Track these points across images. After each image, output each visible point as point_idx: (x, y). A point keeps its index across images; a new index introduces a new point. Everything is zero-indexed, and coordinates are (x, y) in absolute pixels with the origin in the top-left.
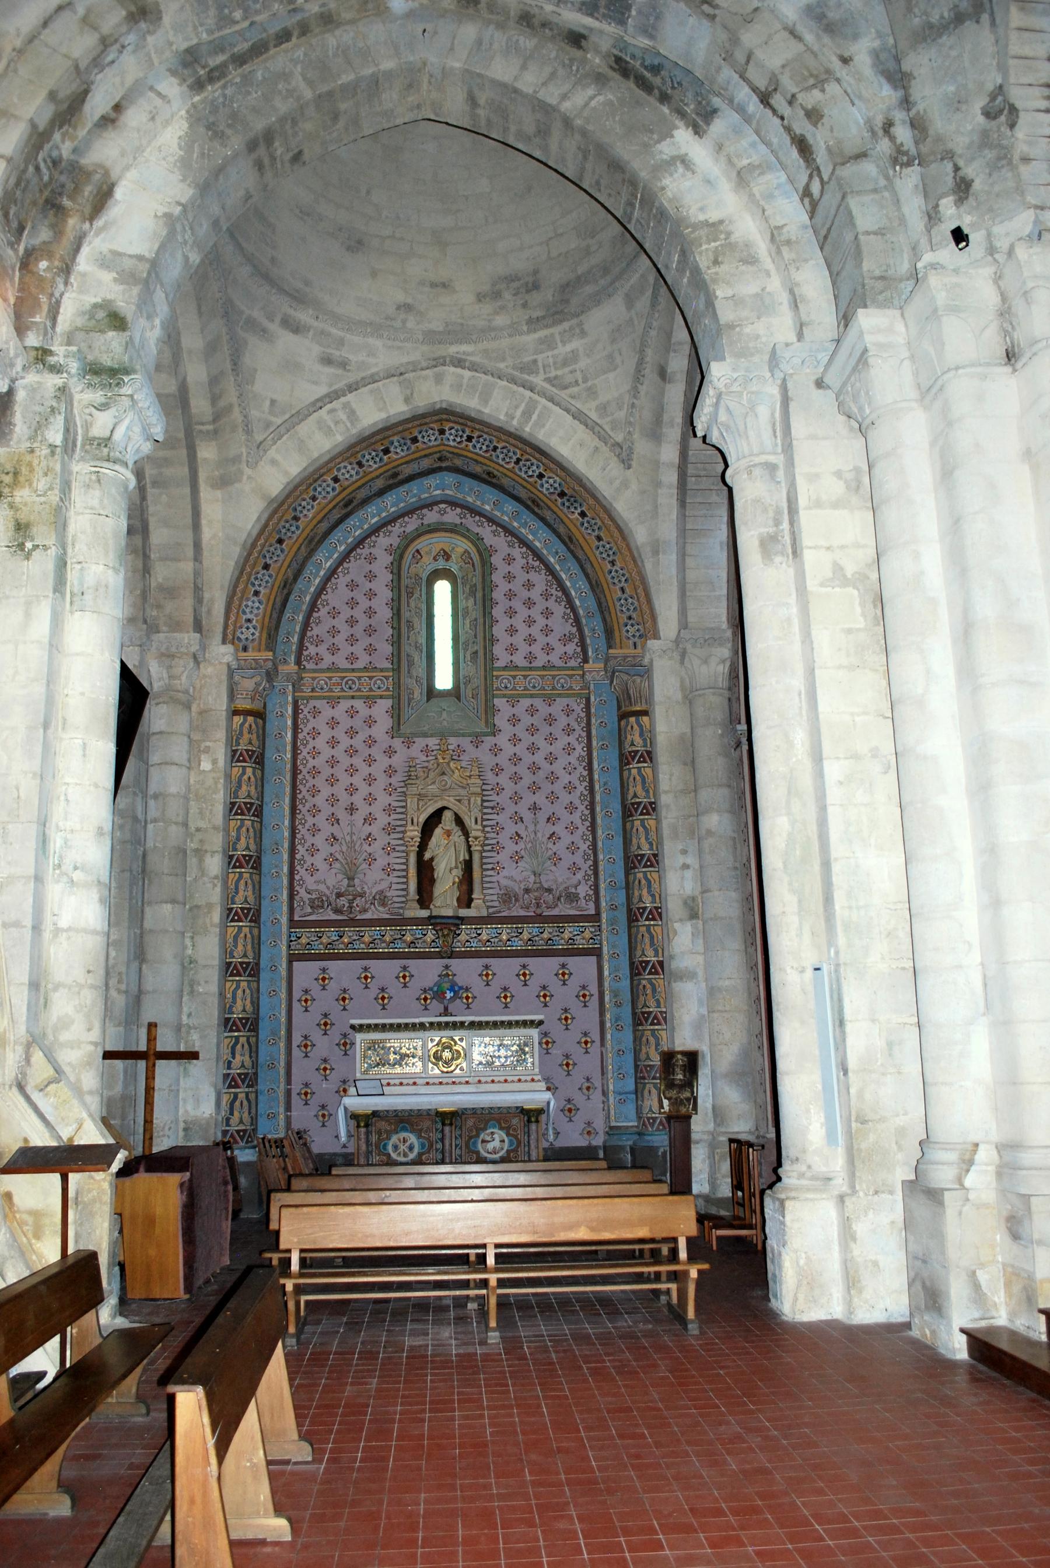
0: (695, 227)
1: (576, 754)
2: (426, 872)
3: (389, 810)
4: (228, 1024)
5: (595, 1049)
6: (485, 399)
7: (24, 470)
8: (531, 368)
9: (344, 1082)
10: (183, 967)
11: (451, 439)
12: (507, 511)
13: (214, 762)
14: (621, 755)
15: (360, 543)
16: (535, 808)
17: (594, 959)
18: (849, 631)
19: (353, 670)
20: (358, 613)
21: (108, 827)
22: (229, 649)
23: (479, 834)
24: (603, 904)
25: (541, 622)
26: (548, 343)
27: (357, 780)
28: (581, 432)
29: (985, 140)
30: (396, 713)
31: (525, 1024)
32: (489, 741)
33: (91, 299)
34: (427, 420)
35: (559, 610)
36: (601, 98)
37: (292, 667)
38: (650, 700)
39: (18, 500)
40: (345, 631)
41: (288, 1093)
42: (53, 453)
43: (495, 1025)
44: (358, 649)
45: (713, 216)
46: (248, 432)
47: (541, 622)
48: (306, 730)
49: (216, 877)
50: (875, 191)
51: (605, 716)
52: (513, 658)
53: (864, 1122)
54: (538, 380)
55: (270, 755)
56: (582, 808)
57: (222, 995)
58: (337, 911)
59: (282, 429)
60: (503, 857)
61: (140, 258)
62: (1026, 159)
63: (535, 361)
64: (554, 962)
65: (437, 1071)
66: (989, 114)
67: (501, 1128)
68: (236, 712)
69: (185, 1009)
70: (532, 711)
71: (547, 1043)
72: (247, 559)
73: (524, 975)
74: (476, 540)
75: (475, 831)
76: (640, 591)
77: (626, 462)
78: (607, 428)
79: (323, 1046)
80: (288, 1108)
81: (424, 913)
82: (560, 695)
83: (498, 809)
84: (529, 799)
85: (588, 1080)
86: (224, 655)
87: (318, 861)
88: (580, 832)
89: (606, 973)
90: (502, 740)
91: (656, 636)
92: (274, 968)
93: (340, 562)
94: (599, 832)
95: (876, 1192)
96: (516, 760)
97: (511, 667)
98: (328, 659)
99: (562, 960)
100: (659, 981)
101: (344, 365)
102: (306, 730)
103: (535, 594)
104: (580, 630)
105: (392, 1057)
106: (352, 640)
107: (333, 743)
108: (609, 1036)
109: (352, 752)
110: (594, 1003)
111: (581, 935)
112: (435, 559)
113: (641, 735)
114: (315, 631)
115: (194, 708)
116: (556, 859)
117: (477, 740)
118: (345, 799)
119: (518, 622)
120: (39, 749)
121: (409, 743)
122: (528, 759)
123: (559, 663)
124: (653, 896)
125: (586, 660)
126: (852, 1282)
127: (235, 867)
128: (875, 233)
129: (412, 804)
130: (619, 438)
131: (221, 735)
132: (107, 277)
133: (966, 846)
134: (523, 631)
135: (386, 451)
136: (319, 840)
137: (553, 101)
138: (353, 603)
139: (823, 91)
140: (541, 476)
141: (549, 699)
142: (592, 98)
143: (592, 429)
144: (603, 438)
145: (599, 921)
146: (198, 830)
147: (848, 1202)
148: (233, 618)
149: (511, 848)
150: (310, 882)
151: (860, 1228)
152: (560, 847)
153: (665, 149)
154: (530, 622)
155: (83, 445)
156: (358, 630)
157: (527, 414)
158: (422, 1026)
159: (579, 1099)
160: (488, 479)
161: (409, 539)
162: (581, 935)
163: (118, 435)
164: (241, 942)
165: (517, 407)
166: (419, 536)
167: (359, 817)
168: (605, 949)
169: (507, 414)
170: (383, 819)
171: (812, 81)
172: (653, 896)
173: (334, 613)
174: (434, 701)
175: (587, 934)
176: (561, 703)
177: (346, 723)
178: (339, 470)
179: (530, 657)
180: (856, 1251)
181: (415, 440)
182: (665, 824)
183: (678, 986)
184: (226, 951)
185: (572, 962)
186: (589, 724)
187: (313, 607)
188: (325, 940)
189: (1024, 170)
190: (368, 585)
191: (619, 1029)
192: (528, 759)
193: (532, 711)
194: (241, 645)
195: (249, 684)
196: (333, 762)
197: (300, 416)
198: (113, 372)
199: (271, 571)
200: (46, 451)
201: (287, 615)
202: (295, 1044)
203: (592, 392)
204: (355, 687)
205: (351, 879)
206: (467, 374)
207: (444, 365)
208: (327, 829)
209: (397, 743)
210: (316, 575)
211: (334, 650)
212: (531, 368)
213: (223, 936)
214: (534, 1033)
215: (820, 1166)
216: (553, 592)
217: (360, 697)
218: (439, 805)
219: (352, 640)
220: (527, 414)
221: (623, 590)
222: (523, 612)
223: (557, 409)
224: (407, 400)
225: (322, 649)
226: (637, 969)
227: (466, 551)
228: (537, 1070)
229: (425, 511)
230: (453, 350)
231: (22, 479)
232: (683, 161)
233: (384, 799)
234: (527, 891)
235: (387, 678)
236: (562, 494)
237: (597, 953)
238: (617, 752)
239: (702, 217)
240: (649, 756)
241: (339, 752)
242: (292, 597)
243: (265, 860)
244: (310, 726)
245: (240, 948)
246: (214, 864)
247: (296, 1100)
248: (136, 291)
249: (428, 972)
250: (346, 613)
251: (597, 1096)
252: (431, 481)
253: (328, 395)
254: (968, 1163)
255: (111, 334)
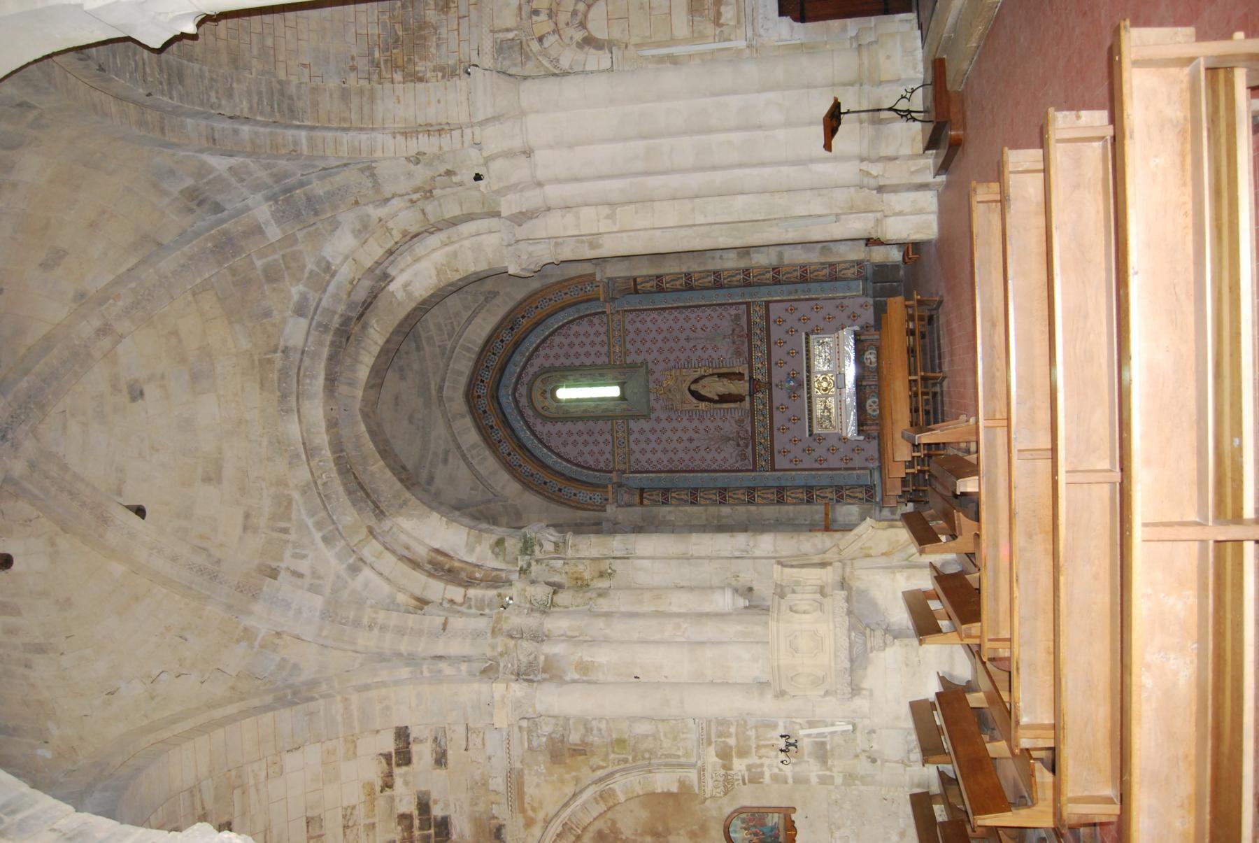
0: (439, 281)
1: (656, 317)
2: (724, 398)
3: (691, 420)
4: (810, 501)
5: (820, 303)
6: (460, 373)
7: (575, 575)
8: (443, 348)
9: (840, 439)
10: (780, 524)
11: (483, 391)
12: (519, 359)
13: (670, 512)
14: (659, 292)
15: (540, 441)
16: (688, 339)
17: (770, 305)
18: (636, 212)
19: (613, 441)
20: (580, 440)
21: (730, 534)
22: (608, 508)
23: (703, 370)
24: (741, 300)
25: (582, 338)
26: (430, 339)
27: (675, 438)
28: (478, 320)
29: (430, 164)
30: (637, 417)
31: (807, 343)
32: (650, 365)
33: (490, 554)
34: (472, 405)
35: (574, 328)
36: (375, 326)
37: (614, 475)
38: (629, 278)
39: (589, 577)
40: (591, 447)
41: (846, 469)
42: (567, 564)
43: (808, 359)
44: (601, 439)
45: (434, 272)
46: (489, 501)
47: (582, 338)
48: (647, 466)
49: (732, 509)
50: (440, 205)
51: (634, 302)
52: (603, 353)
53: (852, 207)
54: (449, 344)
55: (663, 484)
56: (687, 313)
57: (794, 504)
58: (747, 446)
59: (485, 484)
60: (715, 356)
61: (468, 534)
62: (440, 148)
63: (440, 346)
64: (773, 327)
65: (833, 390)
66: (418, 162)
67: (864, 354)
68: (641, 503)
69: (803, 522)
70: (633, 342)
71: (818, 330)
72: (558, 501)
73: (780, 343)
74: (536, 376)
75: (701, 372)
76: (566, 284)
77: (496, 294)
78: (476, 305)
79: (820, 451)
80: (854, 469)
81: (747, 399)
82: (624, 327)
83: (688, 361)
84: (683, 343)
85: (837, 307)
86: (612, 509)
87: (719, 457)
88: (701, 314)
89: (779, 298)
90: (650, 358)
91: (593, 275)
92: (779, 478)
93: (552, 451)
94: (701, 303)
95: (882, 201)
96: (661, 351)
97: (608, 355)
98: (608, 456)
99: (772, 322)
100: (783, 270)
101: (447, 452)
102: (647, 466)
103: (566, 342)
104: (586, 316)
105: (826, 414)
106: (596, 443)
107: (654, 451)
108: (814, 296)
109: (659, 441)
110: (795, 304)
111: (758, 312)
112: (546, 398)
113: (648, 282)
114: (592, 463)
115: (641, 524)
116: (716, 327)
117: (650, 372)
118: (686, 444)
119: (582, 351)
120: (700, 561)
121: (653, 410)
122: (660, 344)
123: (605, 327)
124: (737, 274)
125: (604, 313)
126: (920, 212)
127: (725, 500)
128: (461, 206)
129: (686, 407)
130: (483, 298)
131: (656, 510)
132: (478, 549)
133: (738, 172)
134: (587, 348)
135: (492, 427)
136: (709, 457)
137: (378, 349)
138: (575, 443)
139: (392, 229)
140: (502, 341)
141: (626, 332)
142: (376, 330)
143: (477, 313)
144: (481, 307)
145: (750, 302)
146: (707, 520)
147: (886, 213)
148: (589, 507)
149: (710, 352)
150: (731, 461)
151: (897, 209)
152: (709, 324)
153: (400, 295)
154: (582, 344)
155: (558, 554)
156: (590, 439)
157: (468, 350)
158: (810, 398)
159: (848, 312)
160: (502, 370)
161: (537, 414)
162: (758, 312)
163: (553, 539)
164: (766, 496)
165: (465, 356)
166: (535, 408)
167: (695, 436)
168: (765, 299)
169: (469, 361)
170: (696, 423)
171: (388, 234)
172: (737, 274)
173: (581, 453)
174: (627, 397)
175: (757, 309)
176: (628, 326)
177: (643, 445)
178: (503, 453)
179: (602, 344)
180: (907, 210)
181: (485, 412)
182: (698, 269)
183: (786, 261)
184: (771, 503)
185: (773, 317)
186: (639, 310)
187: (578, 465)
188: (763, 452)
189: (446, 148)
190: (564, 435)
191: (809, 291)
192: (660, 344)
193: (633, 342)
194: (605, 502)
195: (626, 497)
196: (665, 451)
197: (476, 475)
198: (526, 542)
199: (562, 487)
200: (566, 567)
201: (584, 479)
202: (820, 467)
203: (457, 314)
204: (623, 440)
205: (729, 439)
206: (447, 384)
207: (442, 397)
208: (702, 453)
209: (653, 416)
210: (561, 463)
211: (602, 453)
212: (443, 348)
213: (763, 505)
214: (812, 337)
215: (871, 224)
216: (564, 332)
217: (628, 438)
218: (687, 392)
219: (596, 443)
220: (468, 350)
221: (566, 294)
222: (577, 348)
223: (465, 334)
224: (463, 416)
225: (602, 459)
226: (776, 282)
227: (542, 381)
228: (833, 335)
229: (520, 405)
230: (434, 393)
231: (579, 576)
232: (406, 286)
233: (685, 423)
234: (734, 343)
235: (617, 423)
236: (512, 329)
237: (767, 303)
238: (657, 294)
239: (435, 278)
240: (659, 277)
241: (659, 448)
242: (574, 476)
243: (720, 485)
244: (645, 464)
245: (769, 496)
246: (725, 510)
247: (850, 465)
248: (485, 535)
249: (779, 396)
250: (580, 447)
251: (846, 302)
252: (504, 401)
253: (464, 460)
254: (868, 174)
255: (506, 544)
